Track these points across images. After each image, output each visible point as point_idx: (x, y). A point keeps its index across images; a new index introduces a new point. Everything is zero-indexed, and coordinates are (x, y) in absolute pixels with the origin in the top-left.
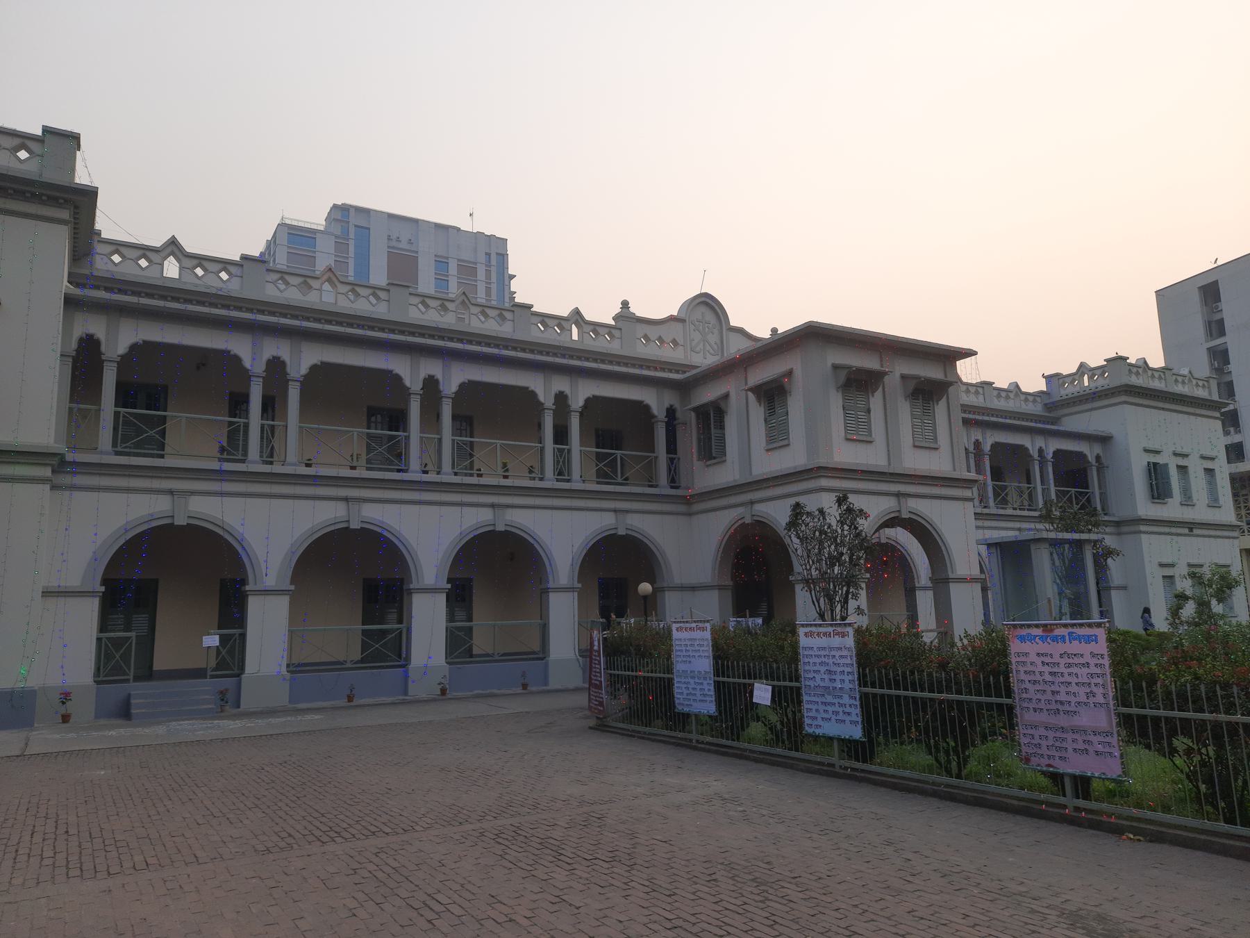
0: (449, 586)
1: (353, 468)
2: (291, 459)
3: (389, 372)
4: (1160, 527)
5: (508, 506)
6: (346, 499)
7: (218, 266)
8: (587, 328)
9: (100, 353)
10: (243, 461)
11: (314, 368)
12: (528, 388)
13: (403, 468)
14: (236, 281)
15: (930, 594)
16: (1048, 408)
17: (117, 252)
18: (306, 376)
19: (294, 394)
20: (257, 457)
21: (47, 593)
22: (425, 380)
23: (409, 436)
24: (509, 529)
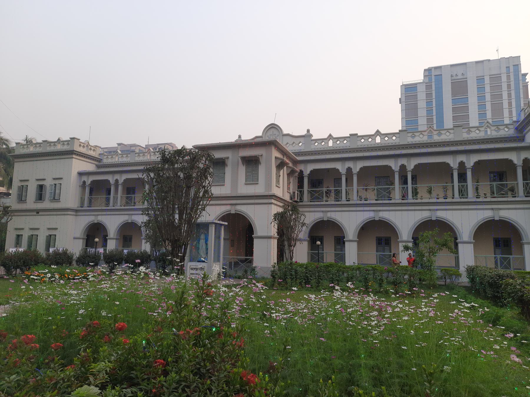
0: (474, 241)
1: (438, 199)
2: (355, 199)
6: (492, 209)
11: (361, 169)
12: (508, 159)
13: (340, 200)
14: (398, 139)
15: (355, 245)
16: (520, 130)
17: (386, 136)
19: (355, 178)
20: (345, 199)
21: (74, 238)
22: (400, 166)
23: (518, 183)
24: (132, 221)
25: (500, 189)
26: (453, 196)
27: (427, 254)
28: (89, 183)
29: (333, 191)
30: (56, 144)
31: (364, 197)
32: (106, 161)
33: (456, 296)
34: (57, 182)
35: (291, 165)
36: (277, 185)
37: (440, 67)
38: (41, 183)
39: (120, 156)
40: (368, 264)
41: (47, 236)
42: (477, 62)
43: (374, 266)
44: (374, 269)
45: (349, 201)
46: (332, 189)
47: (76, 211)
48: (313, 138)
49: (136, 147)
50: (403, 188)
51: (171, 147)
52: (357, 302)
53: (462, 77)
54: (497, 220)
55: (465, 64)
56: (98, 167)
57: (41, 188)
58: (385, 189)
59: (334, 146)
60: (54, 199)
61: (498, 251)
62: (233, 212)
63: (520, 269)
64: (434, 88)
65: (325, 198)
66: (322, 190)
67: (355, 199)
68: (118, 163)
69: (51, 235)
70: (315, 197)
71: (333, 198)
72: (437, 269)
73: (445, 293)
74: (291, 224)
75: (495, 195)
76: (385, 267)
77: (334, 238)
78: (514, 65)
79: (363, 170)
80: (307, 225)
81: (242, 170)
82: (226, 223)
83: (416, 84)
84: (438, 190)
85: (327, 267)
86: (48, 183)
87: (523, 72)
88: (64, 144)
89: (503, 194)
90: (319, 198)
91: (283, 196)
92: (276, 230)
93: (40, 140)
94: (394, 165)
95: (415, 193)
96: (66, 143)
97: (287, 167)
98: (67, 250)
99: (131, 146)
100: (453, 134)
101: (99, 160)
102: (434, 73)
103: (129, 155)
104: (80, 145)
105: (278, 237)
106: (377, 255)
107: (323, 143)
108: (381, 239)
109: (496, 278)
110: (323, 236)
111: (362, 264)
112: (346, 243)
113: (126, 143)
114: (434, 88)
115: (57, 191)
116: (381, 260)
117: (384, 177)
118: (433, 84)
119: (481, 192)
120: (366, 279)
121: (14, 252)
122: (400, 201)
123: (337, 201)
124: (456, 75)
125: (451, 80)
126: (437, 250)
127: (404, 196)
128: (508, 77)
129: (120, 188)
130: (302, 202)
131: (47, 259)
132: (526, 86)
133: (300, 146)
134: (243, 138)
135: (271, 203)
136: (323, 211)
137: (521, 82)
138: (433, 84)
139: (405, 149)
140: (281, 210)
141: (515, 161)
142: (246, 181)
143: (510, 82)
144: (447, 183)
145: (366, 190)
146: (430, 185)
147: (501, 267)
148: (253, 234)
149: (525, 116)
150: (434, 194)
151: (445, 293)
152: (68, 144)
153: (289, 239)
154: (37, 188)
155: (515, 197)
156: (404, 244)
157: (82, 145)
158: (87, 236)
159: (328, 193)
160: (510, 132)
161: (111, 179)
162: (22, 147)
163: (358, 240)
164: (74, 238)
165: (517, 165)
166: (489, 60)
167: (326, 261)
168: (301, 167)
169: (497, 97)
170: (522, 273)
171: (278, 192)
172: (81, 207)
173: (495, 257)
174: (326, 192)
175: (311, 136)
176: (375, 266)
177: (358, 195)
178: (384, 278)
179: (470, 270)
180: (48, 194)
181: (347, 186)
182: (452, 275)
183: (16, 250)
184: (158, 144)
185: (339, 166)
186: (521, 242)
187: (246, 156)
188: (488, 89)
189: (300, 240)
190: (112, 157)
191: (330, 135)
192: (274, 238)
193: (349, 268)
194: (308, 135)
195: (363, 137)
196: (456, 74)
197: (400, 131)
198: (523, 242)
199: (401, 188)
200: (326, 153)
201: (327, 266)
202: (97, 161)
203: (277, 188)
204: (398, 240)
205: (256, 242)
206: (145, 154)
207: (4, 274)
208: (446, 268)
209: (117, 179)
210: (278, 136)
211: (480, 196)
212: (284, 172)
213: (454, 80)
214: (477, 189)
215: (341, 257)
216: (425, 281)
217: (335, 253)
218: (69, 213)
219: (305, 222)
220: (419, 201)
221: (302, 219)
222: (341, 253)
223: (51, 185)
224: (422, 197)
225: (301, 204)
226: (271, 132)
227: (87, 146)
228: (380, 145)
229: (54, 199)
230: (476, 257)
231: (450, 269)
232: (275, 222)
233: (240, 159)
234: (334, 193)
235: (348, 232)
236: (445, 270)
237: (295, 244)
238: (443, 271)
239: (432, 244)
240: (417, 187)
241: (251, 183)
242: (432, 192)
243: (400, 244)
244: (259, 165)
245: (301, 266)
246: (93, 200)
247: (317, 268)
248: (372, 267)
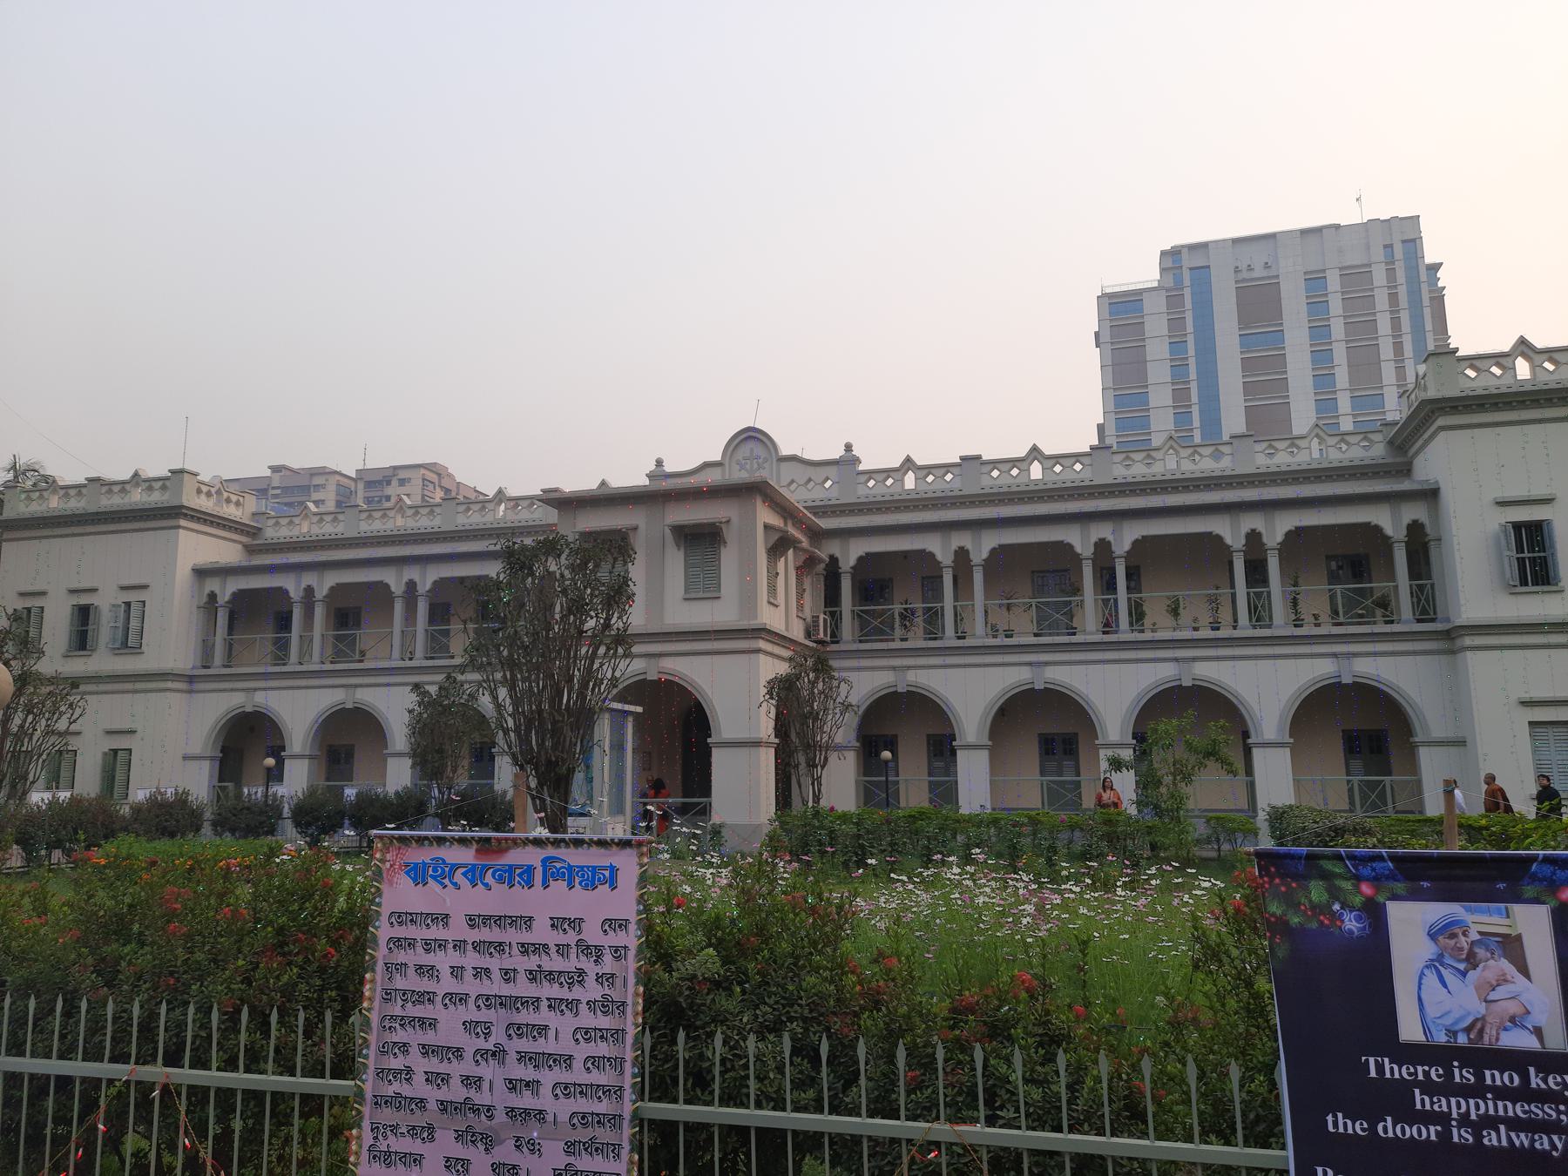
0: (1292, 741)
1: (1196, 629)
2: (978, 633)
3: (1367, 525)
4: (1257, 648)
8: (1538, 359)
12: (1370, 523)
13: (940, 635)
15: (983, 757)
19: (978, 577)
20: (1411, 616)
21: (185, 758)
22: (1096, 544)
23: (1397, 586)
24: (356, 705)
25: (1351, 604)
26: (1236, 621)
27: (1168, 779)
28: (227, 598)
29: (920, 613)
30: (128, 487)
31: (1002, 626)
32: (272, 533)
33: (1194, 871)
34: (132, 597)
35: (805, 543)
36: (772, 600)
37: (1204, 246)
38: (84, 600)
39: (316, 519)
40: (1017, 809)
41: (105, 754)
42: (1305, 232)
43: (1034, 813)
44: (1034, 821)
45: (964, 638)
46: (919, 606)
47: (191, 679)
48: (861, 467)
49: (327, 476)
50: (1105, 602)
51: (435, 476)
52: (993, 890)
53: (1265, 274)
54: (1347, 685)
55: (1271, 237)
56: (250, 550)
57: (84, 614)
58: (1057, 607)
60: (125, 645)
61: (1357, 764)
62: (652, 676)
63: (1412, 812)
64: (1188, 304)
65: (898, 632)
66: (890, 609)
67: (978, 633)
68: (307, 538)
69: (115, 752)
70: (872, 628)
71: (920, 632)
72: (1197, 817)
73: (1171, 865)
74: (813, 708)
75: (1342, 619)
76: (1063, 815)
77: (925, 738)
78: (1404, 242)
79: (999, 553)
80: (856, 709)
81: (675, 562)
82: (639, 709)
83: (1140, 292)
84: (1195, 608)
85: (913, 818)
86: (106, 602)
87: (1430, 258)
88: (150, 488)
89: (1361, 616)
90: (882, 632)
91: (787, 629)
92: (772, 724)
93: (78, 477)
94: (1081, 540)
95: (1137, 615)
96: (157, 485)
97: (795, 548)
98: (188, 794)
99: (312, 475)
100: (1229, 457)
101: (254, 532)
102: (1187, 261)
103: (341, 517)
104: (199, 491)
105: (777, 741)
106: (1042, 785)
107: (890, 482)
108: (1053, 740)
109: (1329, 835)
110: (353, 745)
111: (1004, 809)
112: (958, 752)
113: (295, 465)
114: (1188, 304)
115: (134, 623)
116: (1054, 795)
117: (1054, 571)
118: (1187, 293)
119: (1306, 610)
120: (1015, 848)
121: (47, 802)
122: (1099, 637)
123: (930, 639)
124: (1250, 269)
125: (1237, 282)
126: (1193, 768)
127: (1108, 626)
128: (1391, 273)
129: (319, 612)
130: (837, 642)
131: (136, 819)
132: (1438, 300)
133: (828, 489)
134: (669, 467)
135: (758, 651)
136: (894, 668)
137: (1425, 288)
138: (1187, 293)
139: (1107, 497)
140: (783, 669)
141: (1389, 530)
142: (686, 591)
143: (1396, 287)
144: (1217, 588)
145: (1009, 607)
146: (1176, 593)
147: (1362, 807)
148: (710, 736)
149: (1412, 410)
150: (1186, 616)
151: (1171, 865)
152: (164, 488)
153: (810, 747)
154: (73, 614)
155: (1392, 622)
156: (1110, 753)
157: (205, 489)
159: (907, 616)
160: (1377, 451)
161: (293, 586)
162: (23, 496)
163: (990, 743)
164: (185, 758)
165: (1393, 540)
166: (1337, 227)
167: (907, 802)
168: (833, 548)
169: (1360, 328)
170: (1408, 821)
171: (772, 618)
172: (205, 667)
173: (1348, 782)
174: (901, 615)
175: (857, 460)
176: (1038, 814)
177: (986, 623)
178: (1059, 844)
179: (1278, 817)
180: (105, 628)
181: (956, 599)
182: (1234, 831)
183: (53, 797)
184: (395, 468)
185: (1220, 527)
186: (1411, 740)
188: (1336, 306)
189: (838, 748)
190: (291, 522)
191: (908, 460)
192: (768, 744)
193: (969, 820)
194: (848, 460)
195: (995, 463)
196: (1249, 266)
197: (1092, 448)
198: (1417, 739)
199: (1100, 601)
201: (910, 816)
202: (248, 534)
203: (772, 608)
204: (1097, 742)
205: (719, 758)
206: (388, 512)
207: (19, 865)
208: (1218, 814)
209: (309, 586)
210: (766, 460)
211: (1303, 620)
212: (788, 564)
213: (1244, 280)
214: (1295, 603)
215: (945, 792)
216: (1166, 850)
217: (930, 782)
218: (169, 685)
219: (849, 699)
220: (1147, 636)
221: (843, 695)
222: (947, 782)
223: (114, 606)
224: (1154, 624)
225: (834, 647)
226: (745, 450)
227: (219, 492)
228: (1041, 487)
229: (125, 645)
230: (1297, 782)
231: (1232, 815)
232: (771, 701)
233: (667, 531)
234: (921, 618)
235: (964, 721)
236: (1218, 819)
237: (826, 759)
238: (1212, 822)
239: (1180, 752)
240: (1141, 598)
241: (701, 595)
242: (1181, 610)
243: (1103, 753)
244: (722, 548)
245: (845, 818)
246: (235, 646)
247: (888, 822)
248: (1030, 818)
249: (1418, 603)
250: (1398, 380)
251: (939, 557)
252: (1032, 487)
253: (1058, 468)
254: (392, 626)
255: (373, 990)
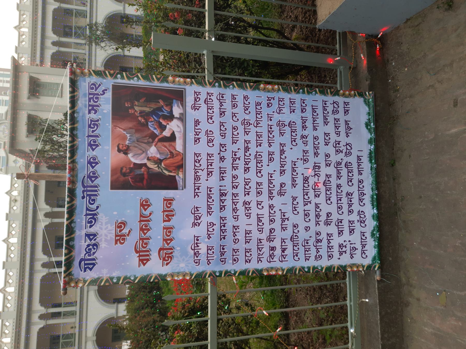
0: (123, 3)
5: (86, 336)
7: (11, 228)
9: (50, 212)
10: (87, 11)
18: (45, 308)
24: (95, 334)
50: (64, 315)
59: (11, 336)
81: (45, 100)
158: (114, 303)
185: (35, 329)
187: (28, 88)
195: (8, 256)
200: (35, 44)
240: (64, 303)
249: (68, 313)
250: (2, 82)
251: (45, 274)
252: (13, 342)
253: (13, 232)
254: (60, 324)
255: (179, 84)
